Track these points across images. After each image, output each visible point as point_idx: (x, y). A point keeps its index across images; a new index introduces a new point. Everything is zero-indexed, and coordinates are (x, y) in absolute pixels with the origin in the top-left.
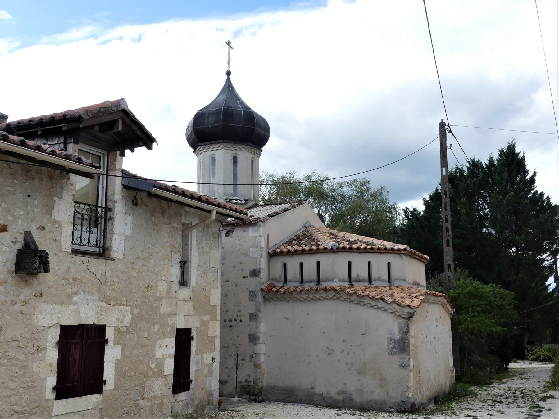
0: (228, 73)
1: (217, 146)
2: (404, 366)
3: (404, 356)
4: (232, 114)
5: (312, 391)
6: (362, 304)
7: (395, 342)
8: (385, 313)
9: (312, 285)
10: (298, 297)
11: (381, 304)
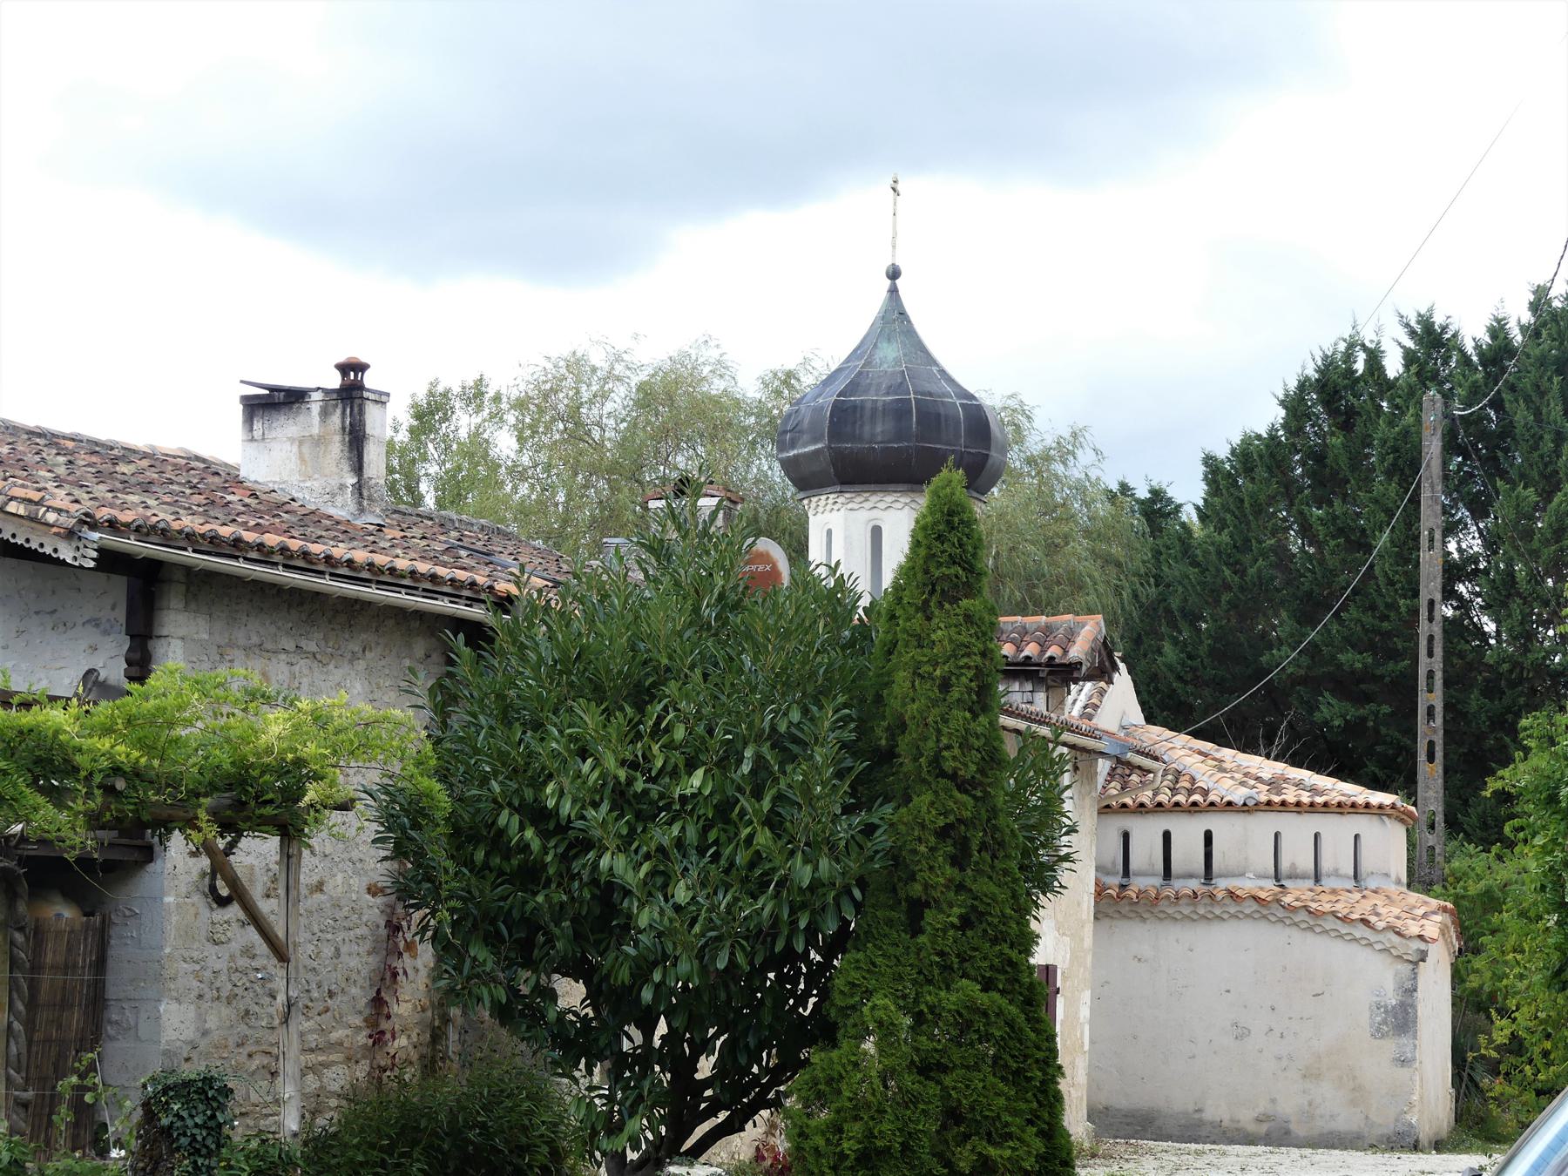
0: (894, 274)
1: (889, 499)
2: (1403, 1062)
3: (1403, 1040)
4: (939, 415)
5: (1197, 1116)
6: (1318, 930)
7: (1386, 1012)
8: (1368, 950)
9: (1195, 884)
10: (1170, 911)
11: (1359, 932)
